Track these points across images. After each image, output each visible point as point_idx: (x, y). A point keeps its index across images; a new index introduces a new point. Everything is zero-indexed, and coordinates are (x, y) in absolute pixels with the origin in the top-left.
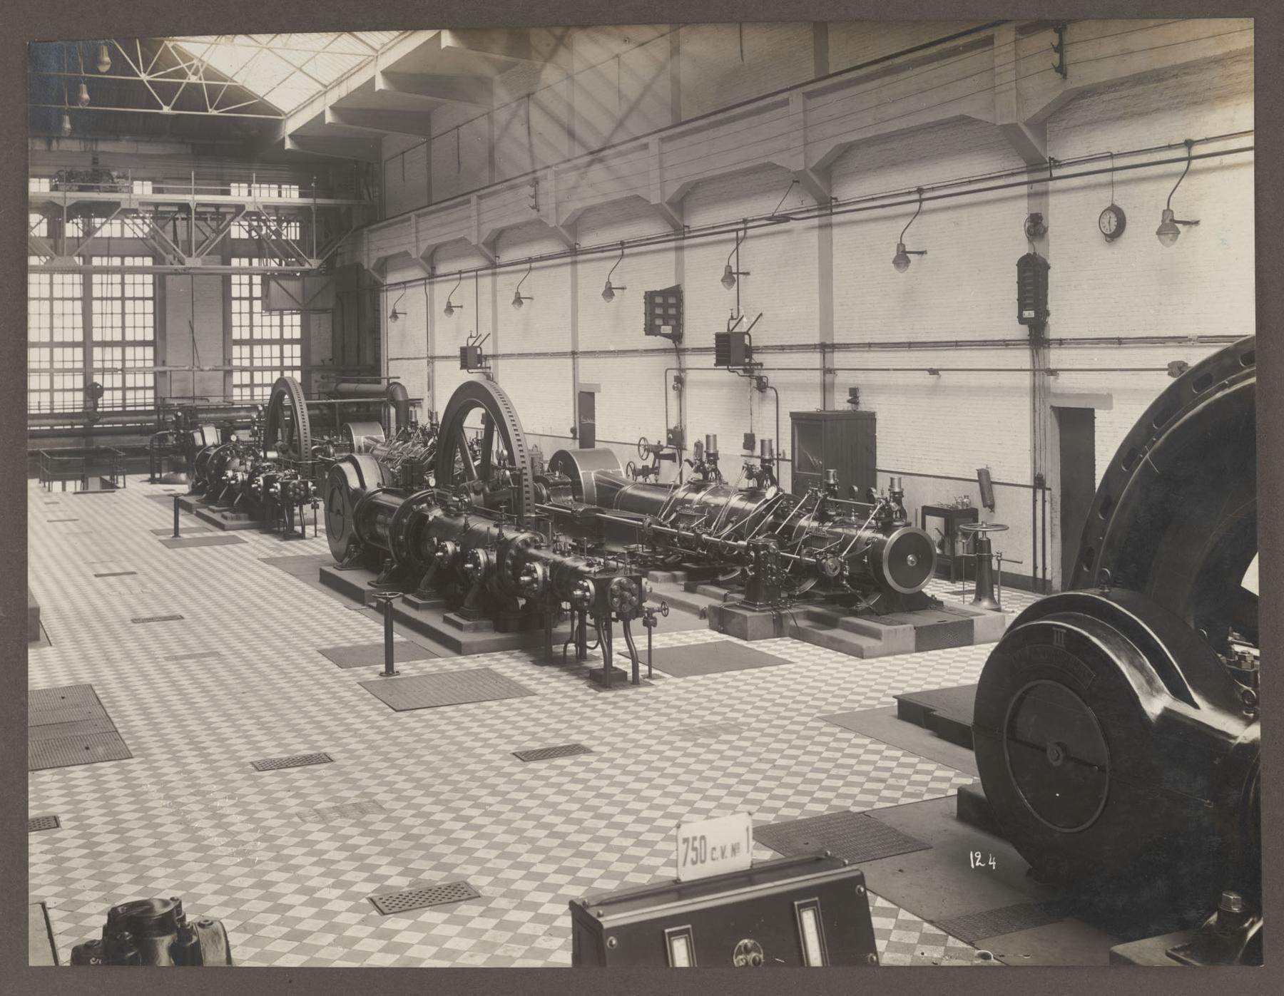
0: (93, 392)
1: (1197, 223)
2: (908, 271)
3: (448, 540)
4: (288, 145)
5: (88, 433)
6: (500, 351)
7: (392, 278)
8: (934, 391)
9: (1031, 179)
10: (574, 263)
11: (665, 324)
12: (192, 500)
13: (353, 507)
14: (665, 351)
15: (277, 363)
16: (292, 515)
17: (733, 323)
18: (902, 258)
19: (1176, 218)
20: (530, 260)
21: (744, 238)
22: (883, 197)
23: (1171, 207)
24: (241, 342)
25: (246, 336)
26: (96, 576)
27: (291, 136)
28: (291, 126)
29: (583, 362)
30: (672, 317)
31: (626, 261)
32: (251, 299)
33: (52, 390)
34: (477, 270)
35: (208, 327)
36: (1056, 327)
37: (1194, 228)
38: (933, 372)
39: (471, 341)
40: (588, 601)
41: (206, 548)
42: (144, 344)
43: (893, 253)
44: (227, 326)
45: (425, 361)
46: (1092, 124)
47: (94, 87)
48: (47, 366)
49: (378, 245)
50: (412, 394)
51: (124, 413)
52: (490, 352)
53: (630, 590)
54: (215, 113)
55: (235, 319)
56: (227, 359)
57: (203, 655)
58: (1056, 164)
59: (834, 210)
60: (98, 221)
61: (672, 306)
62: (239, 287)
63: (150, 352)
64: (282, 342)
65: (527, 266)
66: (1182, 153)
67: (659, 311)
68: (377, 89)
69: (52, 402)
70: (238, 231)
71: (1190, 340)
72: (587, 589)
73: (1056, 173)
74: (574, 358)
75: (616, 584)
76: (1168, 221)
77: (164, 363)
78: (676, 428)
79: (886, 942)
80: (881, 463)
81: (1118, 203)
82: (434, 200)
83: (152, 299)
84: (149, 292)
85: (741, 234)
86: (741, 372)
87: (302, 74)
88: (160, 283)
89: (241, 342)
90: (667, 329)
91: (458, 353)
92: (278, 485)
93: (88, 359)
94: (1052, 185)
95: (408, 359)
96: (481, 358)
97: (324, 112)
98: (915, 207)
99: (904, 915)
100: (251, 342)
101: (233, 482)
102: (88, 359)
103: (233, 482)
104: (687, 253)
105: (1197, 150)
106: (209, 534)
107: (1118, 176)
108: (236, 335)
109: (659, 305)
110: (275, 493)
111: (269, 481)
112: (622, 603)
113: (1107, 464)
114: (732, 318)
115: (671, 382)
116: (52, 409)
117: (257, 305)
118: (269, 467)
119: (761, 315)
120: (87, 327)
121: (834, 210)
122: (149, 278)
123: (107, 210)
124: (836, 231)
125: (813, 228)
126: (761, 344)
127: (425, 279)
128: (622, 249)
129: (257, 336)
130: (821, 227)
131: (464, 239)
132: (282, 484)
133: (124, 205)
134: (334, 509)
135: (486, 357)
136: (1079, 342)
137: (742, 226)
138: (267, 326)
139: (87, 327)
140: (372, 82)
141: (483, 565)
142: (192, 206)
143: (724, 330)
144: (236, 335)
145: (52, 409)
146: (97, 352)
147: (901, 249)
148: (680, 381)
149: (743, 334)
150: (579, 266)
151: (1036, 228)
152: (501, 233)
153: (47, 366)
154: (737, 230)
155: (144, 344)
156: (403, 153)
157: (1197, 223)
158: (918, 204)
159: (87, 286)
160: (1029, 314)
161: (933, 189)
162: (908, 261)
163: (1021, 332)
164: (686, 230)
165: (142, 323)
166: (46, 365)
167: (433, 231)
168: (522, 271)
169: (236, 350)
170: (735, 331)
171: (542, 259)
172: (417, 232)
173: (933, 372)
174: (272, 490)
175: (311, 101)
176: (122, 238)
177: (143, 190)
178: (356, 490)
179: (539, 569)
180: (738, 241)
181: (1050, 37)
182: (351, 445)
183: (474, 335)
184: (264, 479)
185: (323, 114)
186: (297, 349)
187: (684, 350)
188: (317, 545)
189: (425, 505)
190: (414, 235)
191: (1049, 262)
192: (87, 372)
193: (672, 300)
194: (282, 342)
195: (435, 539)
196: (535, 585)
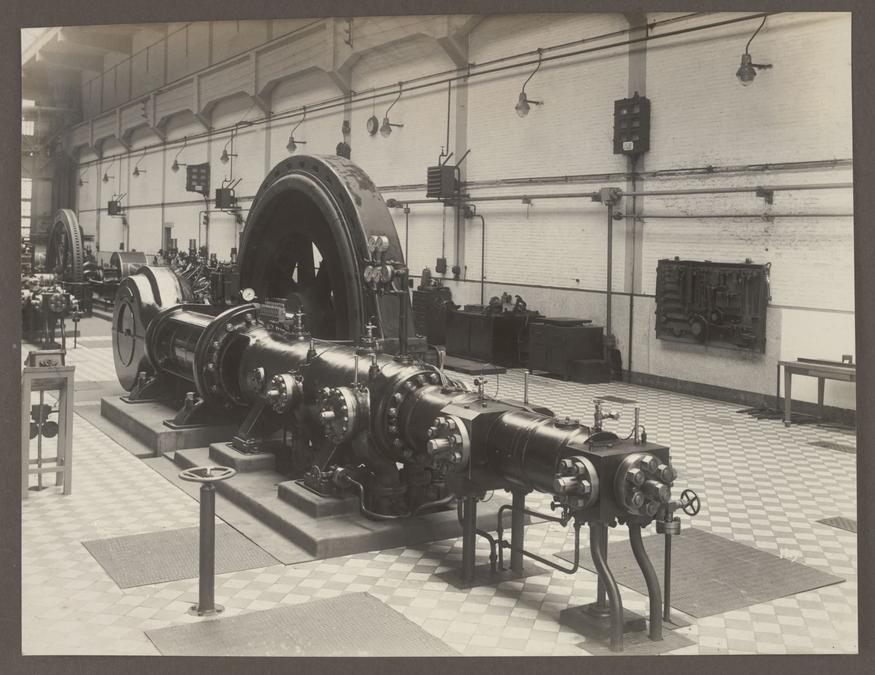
1: (770, 66)
2: (390, 135)
3: (286, 372)
6: (131, 205)
7: (84, 160)
8: (527, 214)
9: (459, 76)
10: (165, 150)
11: (199, 185)
13: (146, 329)
14: (201, 201)
17: (443, 159)
18: (524, 104)
19: (528, 99)
20: (145, 148)
21: (236, 135)
22: (291, 112)
23: (749, 52)
29: (167, 209)
30: (203, 181)
31: (147, 157)
34: (120, 155)
37: (768, 70)
39: (225, 185)
40: (585, 496)
43: (287, 142)
45: (96, 212)
49: (82, 137)
52: (126, 205)
58: (473, 66)
59: (272, 119)
61: (203, 174)
65: (143, 152)
67: (194, 177)
71: (399, 188)
72: (586, 475)
73: (472, 71)
74: (163, 207)
76: (746, 65)
78: (203, 246)
81: (376, 115)
85: (234, 132)
86: (230, 212)
90: (200, 188)
91: (424, 179)
94: (650, 43)
95: (88, 211)
99: (384, 598)
104: (213, 144)
105: (404, 87)
107: (377, 100)
109: (195, 174)
110: (36, 304)
112: (646, 501)
113: (314, 253)
114: (442, 155)
115: (203, 220)
119: (241, 179)
121: (272, 119)
125: (263, 129)
126: (477, 179)
127: (97, 161)
128: (185, 141)
130: (631, 53)
132: (44, 296)
134: (124, 330)
135: (124, 208)
137: (235, 128)
141: (351, 414)
143: (111, 200)
147: (291, 140)
148: (207, 220)
149: (453, 168)
150: (167, 151)
151: (346, 128)
152: (103, 141)
154: (232, 130)
156: (90, 82)
157: (770, 66)
158: (303, 115)
160: (628, 146)
161: (550, 49)
162: (390, 130)
164: (213, 130)
167: (102, 131)
168: (111, 161)
170: (446, 164)
171: (151, 147)
173: (527, 199)
179: (348, 396)
180: (232, 136)
181: (142, 105)
182: (119, 270)
183: (228, 179)
190: (90, 132)
191: (351, 147)
193: (203, 171)
195: (262, 370)
196: (586, 483)
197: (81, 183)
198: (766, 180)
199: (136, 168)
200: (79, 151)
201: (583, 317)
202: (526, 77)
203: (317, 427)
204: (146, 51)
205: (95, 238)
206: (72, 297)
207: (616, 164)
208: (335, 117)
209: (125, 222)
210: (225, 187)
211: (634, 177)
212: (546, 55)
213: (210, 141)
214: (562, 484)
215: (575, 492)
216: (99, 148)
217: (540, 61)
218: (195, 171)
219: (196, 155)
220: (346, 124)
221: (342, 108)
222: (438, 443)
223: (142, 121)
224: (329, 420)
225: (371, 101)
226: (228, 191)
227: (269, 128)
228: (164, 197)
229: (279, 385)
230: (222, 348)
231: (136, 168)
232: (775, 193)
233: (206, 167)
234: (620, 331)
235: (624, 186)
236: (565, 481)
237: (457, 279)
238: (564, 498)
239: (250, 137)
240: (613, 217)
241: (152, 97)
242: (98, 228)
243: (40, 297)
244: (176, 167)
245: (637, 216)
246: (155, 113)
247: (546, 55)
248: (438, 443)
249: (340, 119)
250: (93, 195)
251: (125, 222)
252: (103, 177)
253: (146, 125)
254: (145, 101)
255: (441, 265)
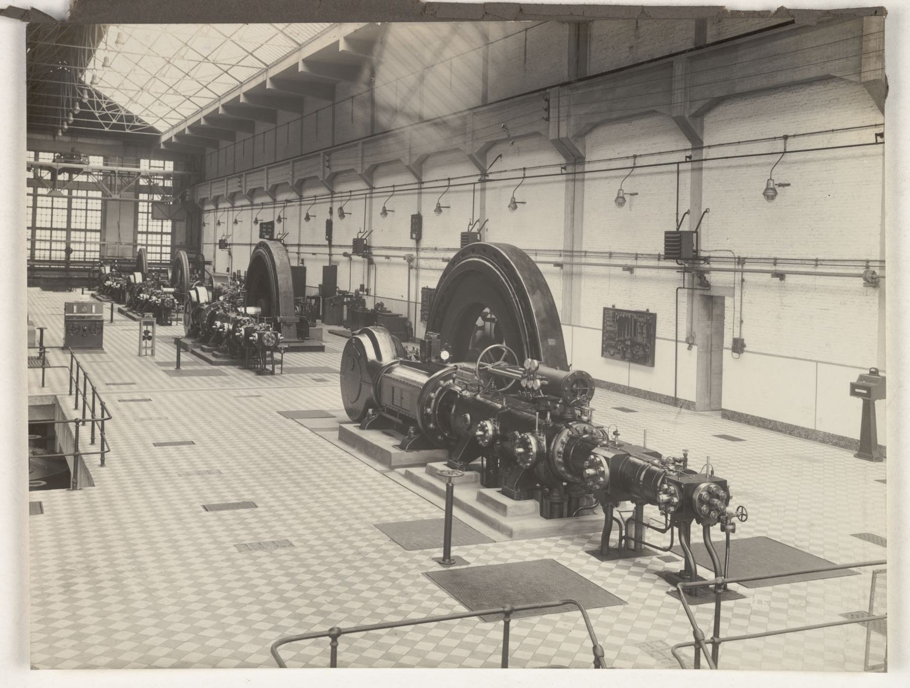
0: (68, 251)
1: (788, 185)
3: (487, 419)
4: (162, 147)
5: (67, 270)
7: (207, 208)
8: (388, 264)
12: (188, 342)
15: (159, 243)
16: (265, 356)
24: (142, 233)
25: (145, 230)
26: (119, 401)
27: (163, 143)
28: (164, 138)
32: (148, 213)
33: (51, 250)
35: (127, 224)
36: (334, 243)
37: (786, 188)
38: (314, 254)
39: (224, 238)
41: (195, 378)
42: (96, 231)
44: (136, 225)
46: (344, 182)
47: (74, 116)
48: (49, 238)
49: (205, 192)
50: (207, 259)
51: (85, 262)
53: (718, 497)
54: (129, 131)
55: (140, 222)
56: (135, 240)
57: (209, 472)
58: (375, 188)
60: (74, 176)
62: (143, 207)
63: (98, 234)
64: (162, 233)
66: (349, 194)
68: (340, 50)
69: (50, 255)
70: (142, 182)
75: (704, 489)
77: (104, 240)
79: (595, 621)
80: (307, 284)
82: (255, 166)
83: (101, 210)
84: (99, 207)
87: (253, 58)
88: (105, 203)
89: (142, 233)
90: (267, 237)
91: (351, 243)
92: (256, 335)
93: (68, 236)
96: (226, 245)
97: (298, 63)
98: (313, 202)
100: (147, 233)
101: (221, 330)
102: (68, 236)
103: (221, 330)
104: (276, 209)
106: (198, 367)
108: (140, 229)
111: (249, 332)
114: (470, 224)
116: (50, 258)
117: (150, 215)
118: (248, 320)
120: (69, 221)
122: (100, 202)
123: (79, 171)
124: (374, 199)
129: (150, 230)
131: (352, 170)
133: (85, 170)
136: (306, 245)
138: (155, 226)
139: (69, 221)
140: (217, 109)
142: (117, 172)
143: (356, 237)
144: (140, 229)
145: (50, 258)
146: (73, 233)
151: (331, 212)
152: (254, 190)
153: (49, 238)
155: (96, 231)
156: (288, 123)
157: (788, 185)
159: (70, 203)
163: (327, 243)
165: (95, 221)
166: (49, 238)
169: (139, 236)
172: (362, 157)
173: (314, 254)
174: (251, 338)
175: (233, 90)
176: (87, 182)
177: (96, 162)
178: (373, 361)
180: (284, 207)
184: (246, 330)
185: (297, 64)
186: (169, 237)
187: (334, 246)
188: (178, 329)
189: (451, 381)
192: (68, 242)
193: (270, 226)
194: (162, 233)
195: (468, 416)
196: (602, 479)
197: (204, 225)
198: (780, 268)
199: (307, 214)
200: (203, 201)
201: (400, 313)
202: (387, 198)
203: (511, 459)
204: (315, 114)
205: (213, 263)
206: (175, 300)
207: (412, 244)
208: (326, 204)
209: (230, 254)
210: (360, 237)
211: (417, 250)
212: (396, 189)
213: (274, 207)
214: (661, 498)
215: (668, 503)
216: (216, 201)
217: (394, 191)
218: (264, 226)
219: (267, 216)
220: (331, 209)
221: (330, 200)
222: (590, 471)
223: (239, 189)
224: (520, 454)
225: (340, 199)
226: (362, 240)
227: (301, 205)
228: (299, 240)
229: (483, 428)
230: (437, 399)
231: (307, 214)
232: (787, 275)
233: (272, 223)
234: (412, 320)
235: (414, 253)
236: (664, 497)
237: (367, 295)
238: (664, 508)
239: (292, 208)
240: (410, 268)
241: (322, 155)
242: (214, 256)
243: (160, 300)
244: (256, 222)
245: (417, 268)
246: (246, 186)
247: (396, 189)
248: (590, 471)
249: (329, 205)
250: (212, 233)
251: (230, 254)
252: (254, 220)
253: (240, 192)
254: (240, 177)
255: (362, 286)
